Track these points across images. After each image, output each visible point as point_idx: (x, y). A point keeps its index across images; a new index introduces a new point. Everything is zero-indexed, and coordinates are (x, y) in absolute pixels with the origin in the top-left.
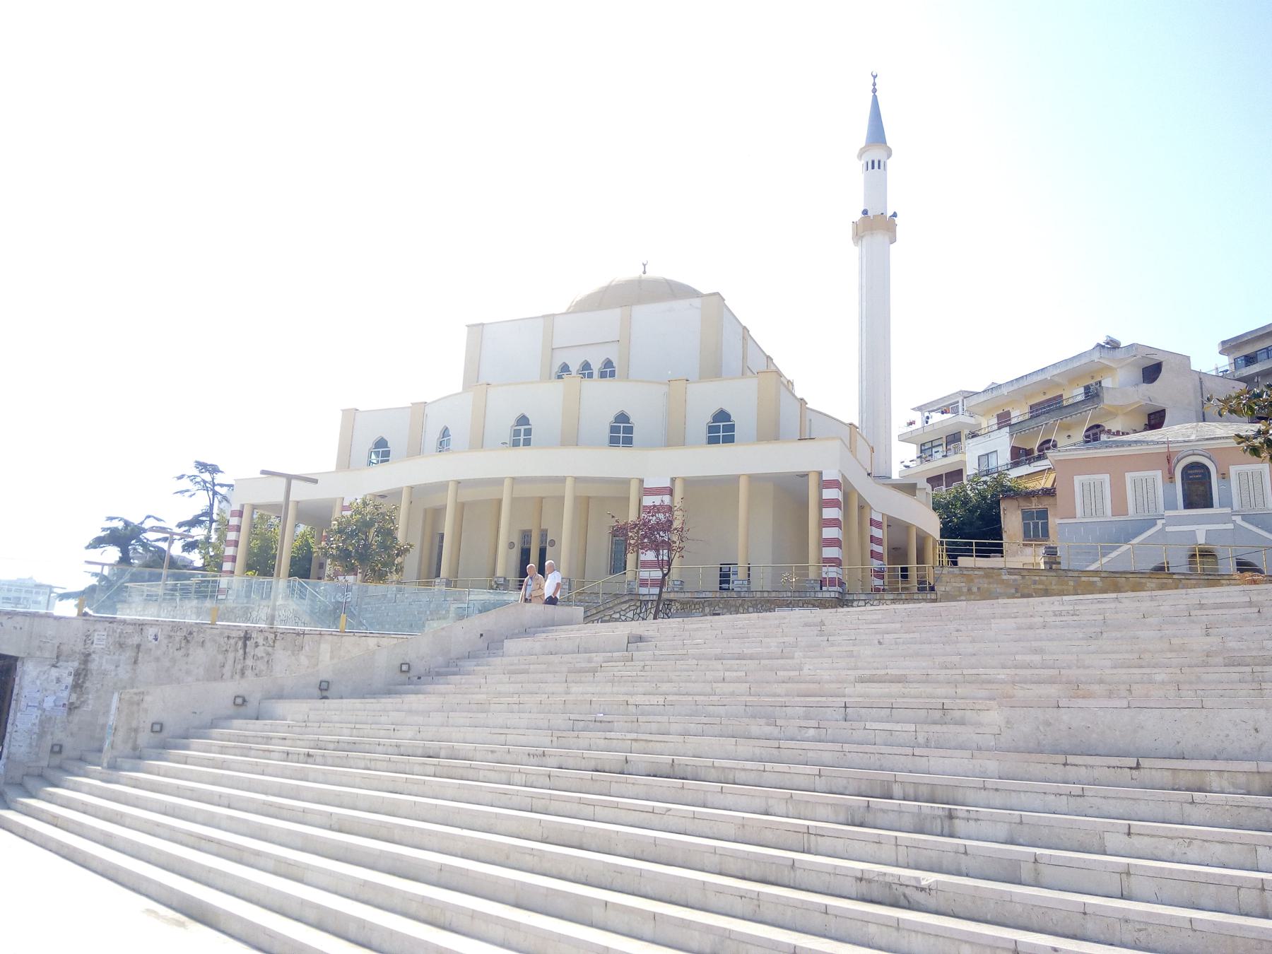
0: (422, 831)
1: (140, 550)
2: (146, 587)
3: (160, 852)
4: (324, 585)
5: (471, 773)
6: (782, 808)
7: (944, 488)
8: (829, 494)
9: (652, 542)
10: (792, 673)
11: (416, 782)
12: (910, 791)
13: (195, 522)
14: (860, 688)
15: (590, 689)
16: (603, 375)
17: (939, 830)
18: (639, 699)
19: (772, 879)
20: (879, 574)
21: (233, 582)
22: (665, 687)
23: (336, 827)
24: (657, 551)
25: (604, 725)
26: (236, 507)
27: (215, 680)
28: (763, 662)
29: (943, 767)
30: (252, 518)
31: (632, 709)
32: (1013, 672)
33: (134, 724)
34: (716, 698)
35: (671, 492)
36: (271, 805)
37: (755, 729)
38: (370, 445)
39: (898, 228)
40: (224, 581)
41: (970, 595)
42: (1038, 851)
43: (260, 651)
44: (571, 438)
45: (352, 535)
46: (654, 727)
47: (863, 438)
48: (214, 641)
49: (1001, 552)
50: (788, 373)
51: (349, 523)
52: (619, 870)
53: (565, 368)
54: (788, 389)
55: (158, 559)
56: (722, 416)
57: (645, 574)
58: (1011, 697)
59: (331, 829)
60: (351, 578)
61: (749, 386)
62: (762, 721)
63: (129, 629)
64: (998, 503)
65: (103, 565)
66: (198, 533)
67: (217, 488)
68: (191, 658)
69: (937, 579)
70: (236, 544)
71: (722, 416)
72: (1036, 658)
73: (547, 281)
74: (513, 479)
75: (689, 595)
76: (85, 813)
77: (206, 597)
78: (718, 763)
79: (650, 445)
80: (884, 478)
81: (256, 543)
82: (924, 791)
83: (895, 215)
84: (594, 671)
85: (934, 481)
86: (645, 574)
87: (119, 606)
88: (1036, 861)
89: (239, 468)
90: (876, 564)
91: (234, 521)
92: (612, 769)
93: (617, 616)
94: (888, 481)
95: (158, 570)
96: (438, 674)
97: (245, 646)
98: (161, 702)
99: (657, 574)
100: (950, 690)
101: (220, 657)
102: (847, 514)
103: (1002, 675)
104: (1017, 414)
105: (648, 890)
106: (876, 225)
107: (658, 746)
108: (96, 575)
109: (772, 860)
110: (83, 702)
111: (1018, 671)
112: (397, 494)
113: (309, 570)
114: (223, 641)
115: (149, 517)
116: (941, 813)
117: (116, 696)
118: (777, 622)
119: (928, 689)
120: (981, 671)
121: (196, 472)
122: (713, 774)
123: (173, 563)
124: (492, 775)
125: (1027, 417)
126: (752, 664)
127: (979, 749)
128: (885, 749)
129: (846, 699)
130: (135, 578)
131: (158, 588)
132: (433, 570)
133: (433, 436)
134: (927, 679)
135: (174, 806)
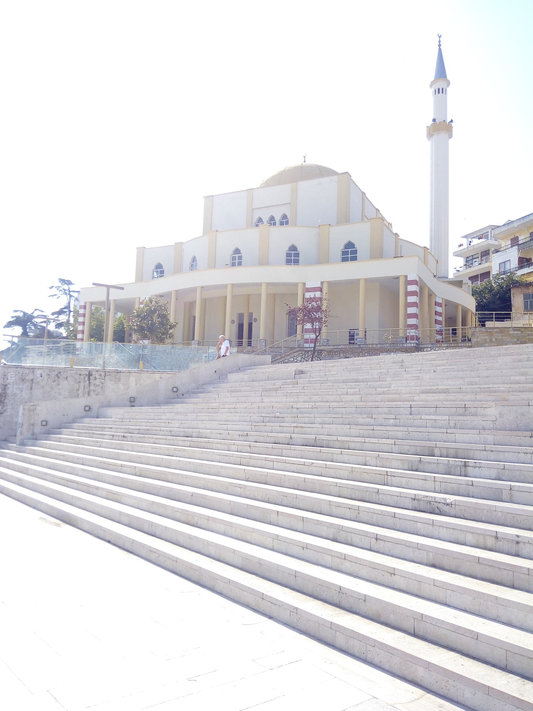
0: (182, 475)
1: (33, 328)
2: (37, 348)
3: (47, 488)
4: (132, 345)
5: (209, 445)
6: (374, 462)
7: (479, 283)
8: (411, 288)
9: (309, 318)
10: (385, 389)
11: (180, 450)
12: (444, 452)
13: (61, 312)
14: (423, 396)
15: (274, 400)
16: (282, 224)
17: (459, 473)
18: (299, 405)
19: (367, 499)
20: (440, 332)
21: (83, 345)
22: (315, 398)
23: (138, 474)
24: (313, 323)
25: (279, 419)
26: (82, 304)
27: (74, 397)
28: (369, 383)
29: (463, 439)
30: (91, 310)
31: (295, 410)
32: (509, 386)
33: (32, 422)
34: (343, 404)
35: (321, 290)
36: (105, 463)
37: (361, 421)
38: (153, 267)
39: (454, 129)
40: (78, 344)
41: (491, 343)
42: (513, 484)
43: (97, 382)
44: (264, 261)
45: (144, 318)
46: (307, 420)
47: (432, 256)
48: (73, 376)
49: (510, 318)
50: (389, 218)
51: (142, 311)
52: (286, 495)
53: (260, 220)
54: (388, 228)
55: (43, 334)
56: (350, 245)
57: (307, 336)
58: (507, 400)
59: (135, 475)
60: (146, 342)
61: (366, 227)
62: (365, 416)
63: (27, 371)
64: (510, 290)
65: (13, 336)
66: (63, 318)
67: (72, 293)
68: (60, 386)
69: (473, 334)
70: (83, 324)
71: (350, 245)
72: (523, 378)
73: (248, 168)
74: (233, 285)
75: (332, 347)
76: (8, 468)
77: (69, 353)
78: (340, 438)
79: (309, 263)
80: (444, 278)
81: (94, 323)
82: (452, 452)
83: (452, 121)
84: (276, 390)
85: (473, 279)
86: (307, 336)
87: (23, 358)
88: (511, 489)
89: (81, 282)
90: (438, 327)
91: (81, 311)
92: (284, 442)
93: (292, 359)
94: (446, 280)
95: (42, 339)
96: (193, 393)
97: (89, 379)
98: (46, 410)
99: (313, 336)
100: (473, 397)
101: (76, 386)
102: (421, 300)
103: (502, 387)
104: (523, 238)
105: (301, 505)
106: (441, 128)
107: (309, 430)
108: (9, 342)
109: (367, 490)
110: (5, 410)
111: (512, 386)
112: (169, 294)
113: (124, 337)
114: (77, 377)
115: (36, 310)
116: (460, 464)
117: (21, 407)
118: (377, 361)
119: (460, 396)
120: (491, 386)
121: (60, 284)
122: (338, 444)
123: (50, 335)
124: (219, 446)
125: (528, 239)
126: (363, 385)
127: (484, 429)
128: (431, 430)
129: (412, 403)
130: (33, 343)
131: (44, 348)
132: (190, 337)
133: (187, 261)
134: (460, 391)
135: (54, 464)
